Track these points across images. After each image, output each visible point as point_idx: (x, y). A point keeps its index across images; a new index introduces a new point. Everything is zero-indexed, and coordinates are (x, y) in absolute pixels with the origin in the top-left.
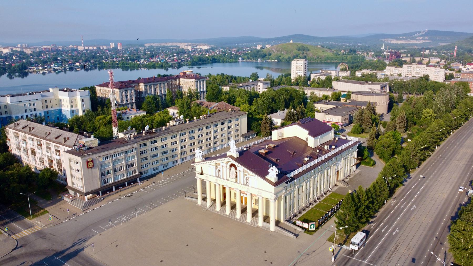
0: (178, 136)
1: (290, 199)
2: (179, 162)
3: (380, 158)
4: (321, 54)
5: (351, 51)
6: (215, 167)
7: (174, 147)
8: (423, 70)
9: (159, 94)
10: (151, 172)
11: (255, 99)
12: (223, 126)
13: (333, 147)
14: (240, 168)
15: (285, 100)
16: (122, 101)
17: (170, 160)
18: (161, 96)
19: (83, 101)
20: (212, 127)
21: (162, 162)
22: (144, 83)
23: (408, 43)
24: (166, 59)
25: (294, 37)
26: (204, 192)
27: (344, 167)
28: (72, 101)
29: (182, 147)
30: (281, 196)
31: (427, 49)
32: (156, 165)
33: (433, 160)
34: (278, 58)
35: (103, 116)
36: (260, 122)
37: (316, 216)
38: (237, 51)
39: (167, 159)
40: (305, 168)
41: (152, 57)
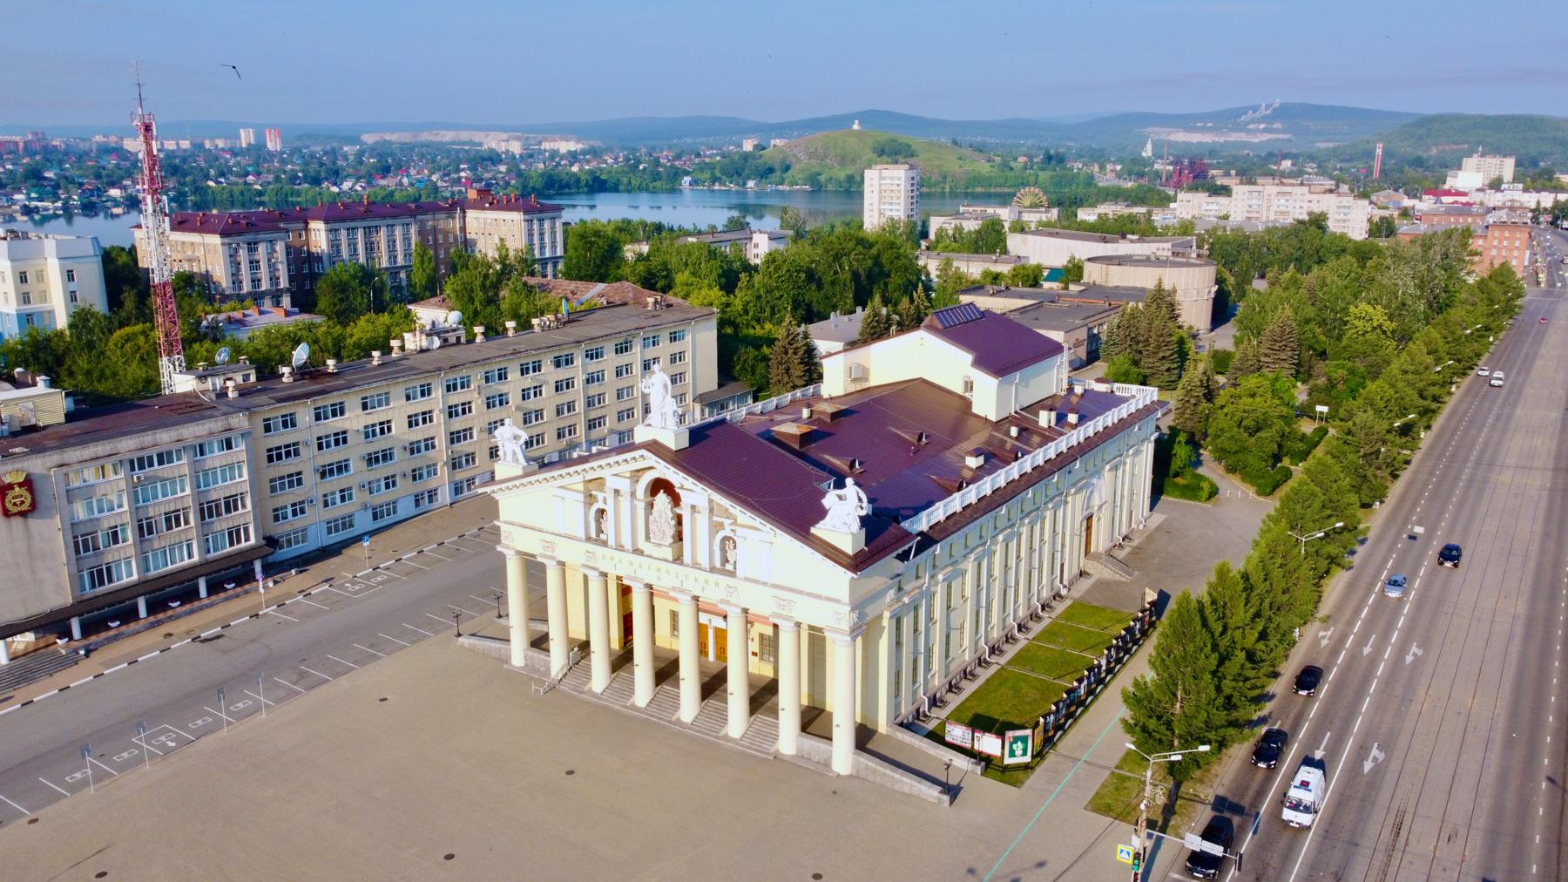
0: (438, 392)
1: (916, 630)
2: (445, 496)
3: (1231, 470)
4: (952, 165)
5: (1049, 158)
6: (581, 497)
7: (420, 433)
8: (1298, 204)
9: (385, 264)
10: (318, 538)
11: (742, 275)
12: (624, 359)
13: (1072, 418)
14: (695, 493)
15: (856, 276)
16: (237, 283)
17: (405, 488)
18: (394, 271)
19: (70, 276)
20: (579, 361)
21: (365, 497)
22: (326, 221)
23: (1222, 140)
24: (434, 178)
25: (867, 117)
26: (537, 610)
27: (1110, 501)
28: (23, 278)
29: (454, 437)
30: (880, 617)
31: (1285, 157)
32: (339, 510)
33: (1422, 477)
34: (813, 180)
35: (139, 328)
36: (765, 350)
37: (1024, 701)
38: (678, 157)
39: (390, 483)
40: (971, 495)
41: (385, 171)
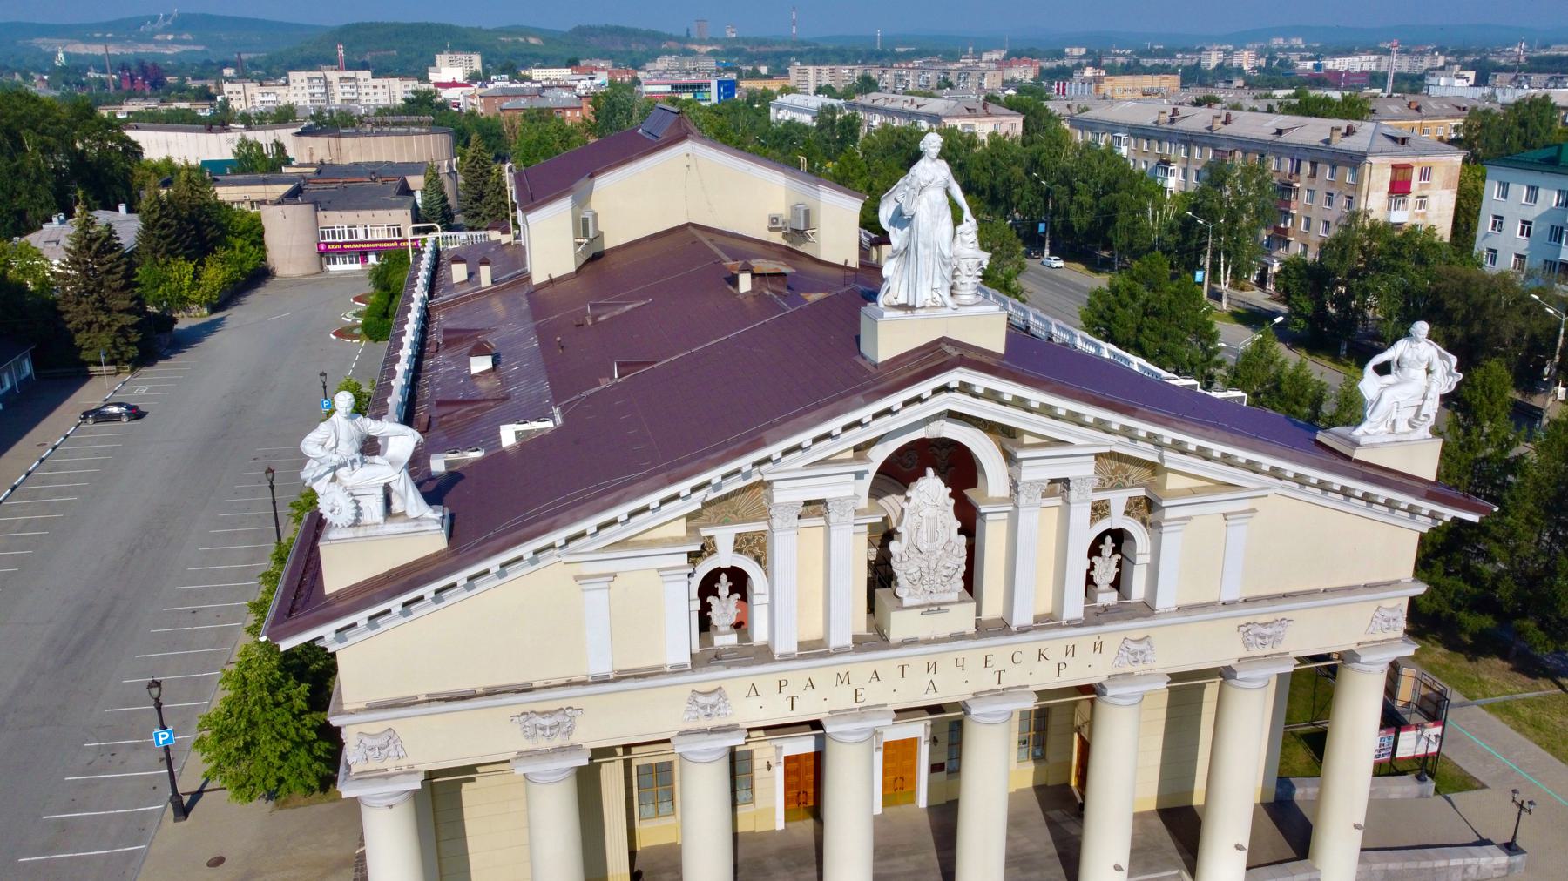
23: (131, 51)
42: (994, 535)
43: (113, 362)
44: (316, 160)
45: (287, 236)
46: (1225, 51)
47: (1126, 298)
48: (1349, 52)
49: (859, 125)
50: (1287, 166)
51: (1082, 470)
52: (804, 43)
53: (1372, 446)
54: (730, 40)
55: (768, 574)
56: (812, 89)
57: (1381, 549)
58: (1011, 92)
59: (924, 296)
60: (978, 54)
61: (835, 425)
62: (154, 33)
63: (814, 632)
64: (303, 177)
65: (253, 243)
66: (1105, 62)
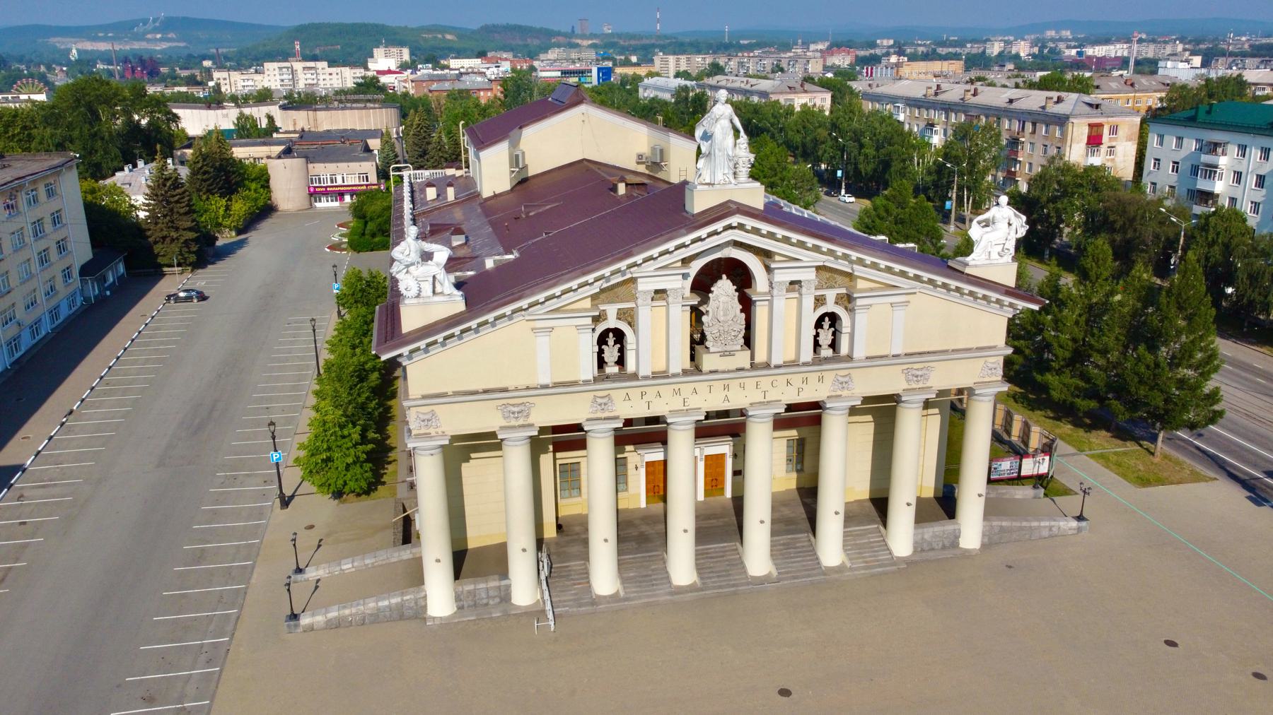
23: (128, 48)
42: (760, 313)
43: (179, 265)
44: (298, 128)
45: (286, 182)
46: (1005, 42)
47: (883, 214)
48: (1106, 41)
49: (707, 100)
50: (1016, 126)
51: (809, 276)
52: (666, 37)
53: (976, 266)
54: (607, 35)
55: (635, 332)
56: (672, 73)
57: (989, 328)
58: (830, 75)
59: (719, 177)
60: (806, 45)
61: (671, 245)
62: (145, 34)
63: (661, 366)
64: (291, 140)
65: (262, 186)
66: (908, 51)
